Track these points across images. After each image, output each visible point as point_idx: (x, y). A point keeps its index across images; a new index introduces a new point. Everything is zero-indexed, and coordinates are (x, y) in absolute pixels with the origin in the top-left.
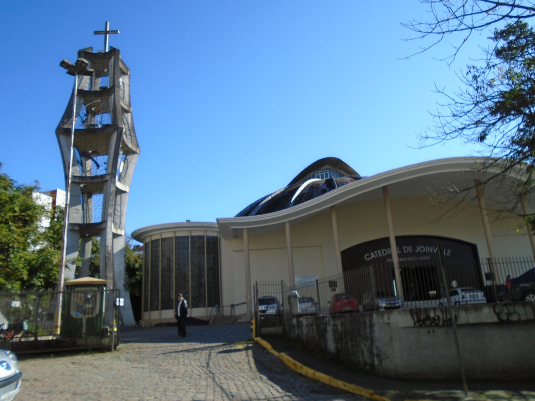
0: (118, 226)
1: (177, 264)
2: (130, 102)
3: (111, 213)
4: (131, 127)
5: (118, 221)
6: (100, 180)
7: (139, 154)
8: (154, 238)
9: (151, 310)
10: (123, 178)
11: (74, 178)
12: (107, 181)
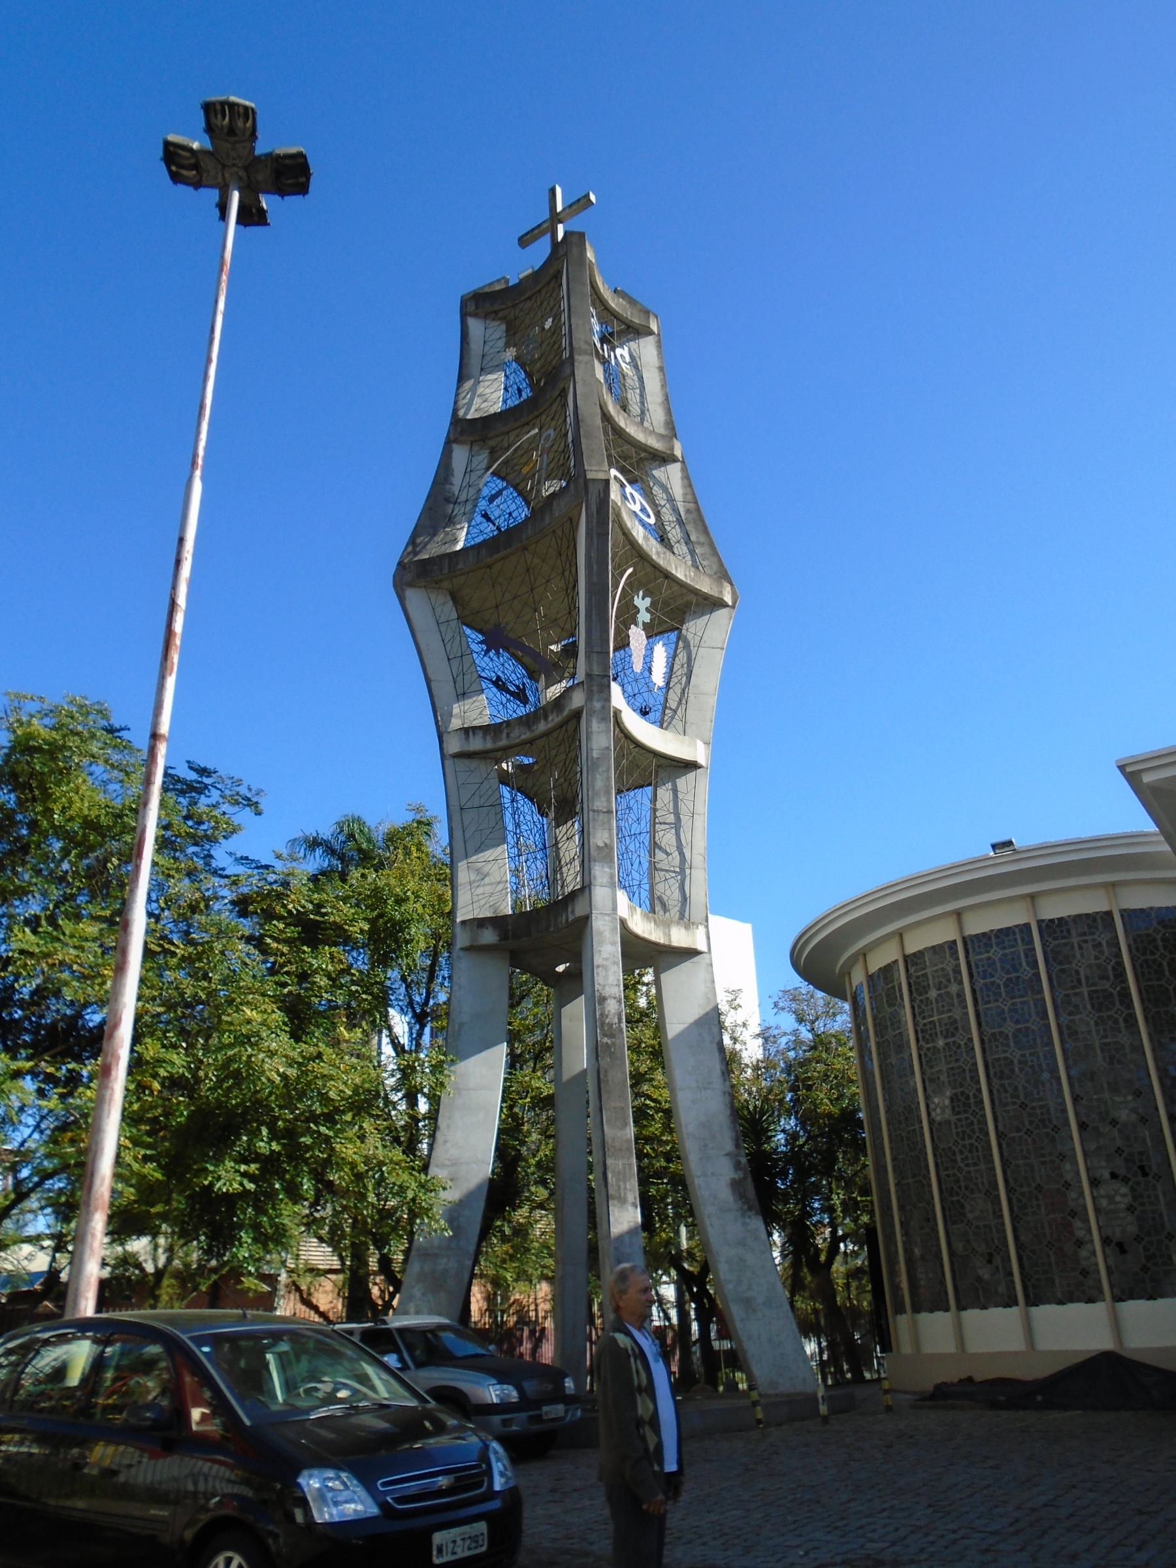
0: (674, 912)
1: (998, 1071)
2: (670, 424)
3: (608, 847)
4: (688, 511)
5: (669, 890)
6: (554, 719)
7: (733, 607)
8: (877, 962)
9: (917, 1309)
10: (675, 711)
12: (577, 715)
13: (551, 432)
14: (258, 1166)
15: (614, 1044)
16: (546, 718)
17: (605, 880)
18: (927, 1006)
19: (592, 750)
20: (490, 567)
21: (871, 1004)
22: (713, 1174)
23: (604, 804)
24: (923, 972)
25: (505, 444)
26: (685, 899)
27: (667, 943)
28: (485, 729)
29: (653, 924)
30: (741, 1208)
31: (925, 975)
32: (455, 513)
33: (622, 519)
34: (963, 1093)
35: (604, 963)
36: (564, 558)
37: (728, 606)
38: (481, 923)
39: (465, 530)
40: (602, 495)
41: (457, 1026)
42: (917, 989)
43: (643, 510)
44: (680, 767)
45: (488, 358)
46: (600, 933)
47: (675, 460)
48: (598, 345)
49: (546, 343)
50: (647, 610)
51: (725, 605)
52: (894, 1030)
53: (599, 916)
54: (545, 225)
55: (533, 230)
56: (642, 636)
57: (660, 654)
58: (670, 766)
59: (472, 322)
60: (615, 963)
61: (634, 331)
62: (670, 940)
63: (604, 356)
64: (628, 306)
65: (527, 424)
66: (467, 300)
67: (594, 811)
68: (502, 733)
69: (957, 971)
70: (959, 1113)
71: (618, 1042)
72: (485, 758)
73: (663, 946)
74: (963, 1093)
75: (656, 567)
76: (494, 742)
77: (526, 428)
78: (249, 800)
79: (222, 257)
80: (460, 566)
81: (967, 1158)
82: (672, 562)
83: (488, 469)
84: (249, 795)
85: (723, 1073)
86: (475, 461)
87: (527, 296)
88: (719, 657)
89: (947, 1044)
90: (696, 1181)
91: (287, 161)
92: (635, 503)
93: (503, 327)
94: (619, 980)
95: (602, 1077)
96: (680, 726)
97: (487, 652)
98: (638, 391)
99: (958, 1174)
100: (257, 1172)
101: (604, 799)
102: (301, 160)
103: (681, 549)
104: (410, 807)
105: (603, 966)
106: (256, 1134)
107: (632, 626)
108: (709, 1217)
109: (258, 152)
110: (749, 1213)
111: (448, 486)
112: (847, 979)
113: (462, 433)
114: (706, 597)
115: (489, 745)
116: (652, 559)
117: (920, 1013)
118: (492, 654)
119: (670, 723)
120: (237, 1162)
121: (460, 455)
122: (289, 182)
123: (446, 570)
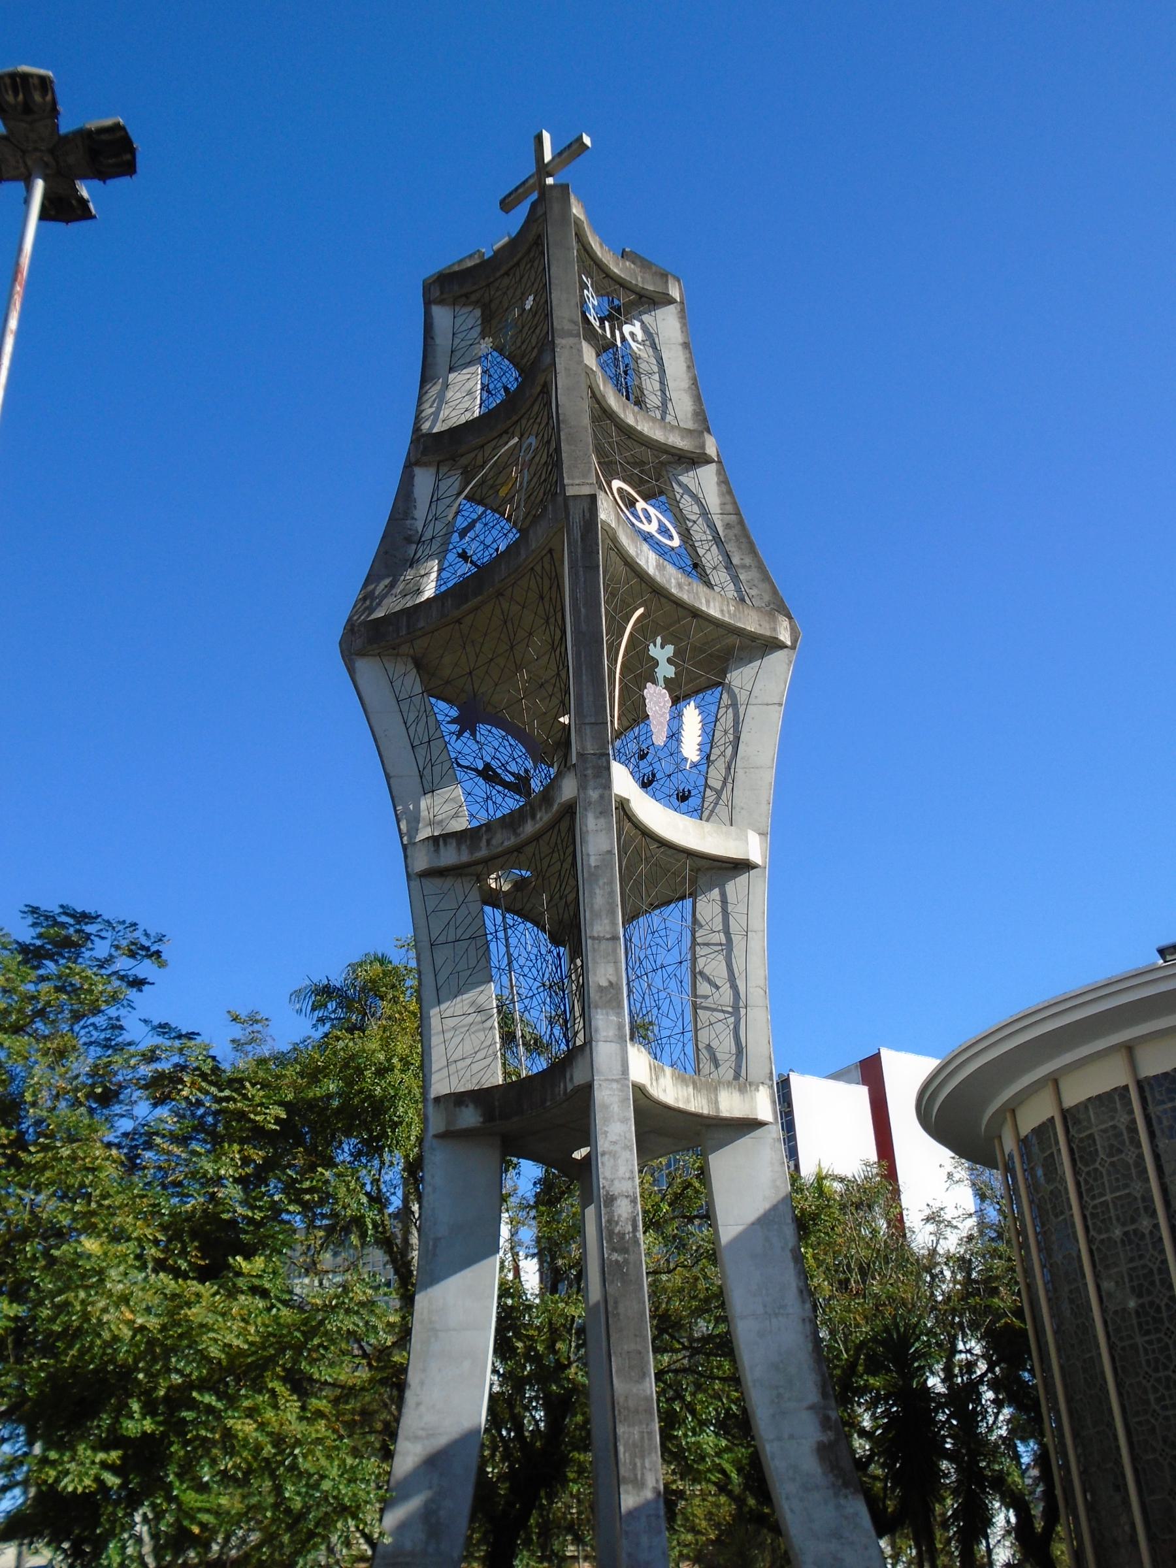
2: (701, 415)
3: (614, 986)
4: (728, 526)
6: (544, 817)
7: (793, 647)
10: (719, 793)
11: (437, 850)
13: (532, 440)
14: (120, 1453)
15: (626, 1261)
16: (533, 817)
17: (611, 1033)
18: (1095, 1180)
19: (588, 855)
20: (459, 621)
21: (1027, 1179)
22: (791, 1437)
23: (608, 928)
24: (1089, 1132)
25: (479, 461)
26: (740, 1051)
27: (712, 1113)
28: (460, 837)
29: (691, 1089)
30: (833, 1485)
31: (1091, 1136)
32: (417, 557)
33: (622, 546)
34: (1152, 1303)
35: (612, 1148)
36: (547, 599)
37: (786, 647)
38: (459, 1099)
39: (434, 575)
40: (587, 515)
41: (431, 1243)
42: (1081, 1157)
43: (663, 530)
44: (726, 869)
45: (458, 354)
46: (606, 1107)
47: (708, 461)
48: (596, 324)
49: (526, 328)
50: (669, 661)
51: (781, 646)
52: (1056, 1216)
53: (604, 1084)
54: (531, 181)
55: (517, 189)
56: (663, 696)
57: (691, 716)
58: (712, 869)
59: (436, 310)
60: (627, 1147)
61: (651, 301)
62: (718, 1109)
63: (604, 337)
64: (637, 270)
65: (506, 432)
66: (430, 284)
67: (593, 938)
68: (480, 839)
69: (1132, 1129)
70: (1148, 1333)
71: (632, 1258)
72: (461, 875)
73: (708, 1117)
74: (1152, 1303)
75: (678, 604)
76: (472, 854)
77: (505, 438)
78: (148, 949)
79: (17, 264)
80: (422, 624)
81: (1162, 1398)
82: (701, 595)
83: (459, 494)
84: (147, 944)
85: (801, 1292)
86: (443, 485)
87: (502, 271)
88: (776, 717)
89: (1126, 1234)
90: (768, 1447)
91: (104, 137)
92: (650, 521)
93: (478, 312)
94: (632, 1172)
95: (610, 1309)
96: (725, 816)
97: (459, 735)
98: (656, 377)
99: (1153, 1421)
100: (118, 1462)
101: (606, 921)
102: (119, 134)
103: (720, 577)
104: (399, 943)
105: (610, 1153)
106: (122, 1410)
107: (649, 684)
108: (787, 1498)
109: (63, 130)
110: (844, 1491)
111: (408, 522)
112: (996, 1142)
113: (424, 453)
114: (753, 637)
115: (465, 857)
116: (672, 595)
117: (1088, 1191)
118: (467, 734)
119: (712, 811)
120: (95, 1449)
121: (424, 480)
122: (111, 161)
123: (404, 632)
